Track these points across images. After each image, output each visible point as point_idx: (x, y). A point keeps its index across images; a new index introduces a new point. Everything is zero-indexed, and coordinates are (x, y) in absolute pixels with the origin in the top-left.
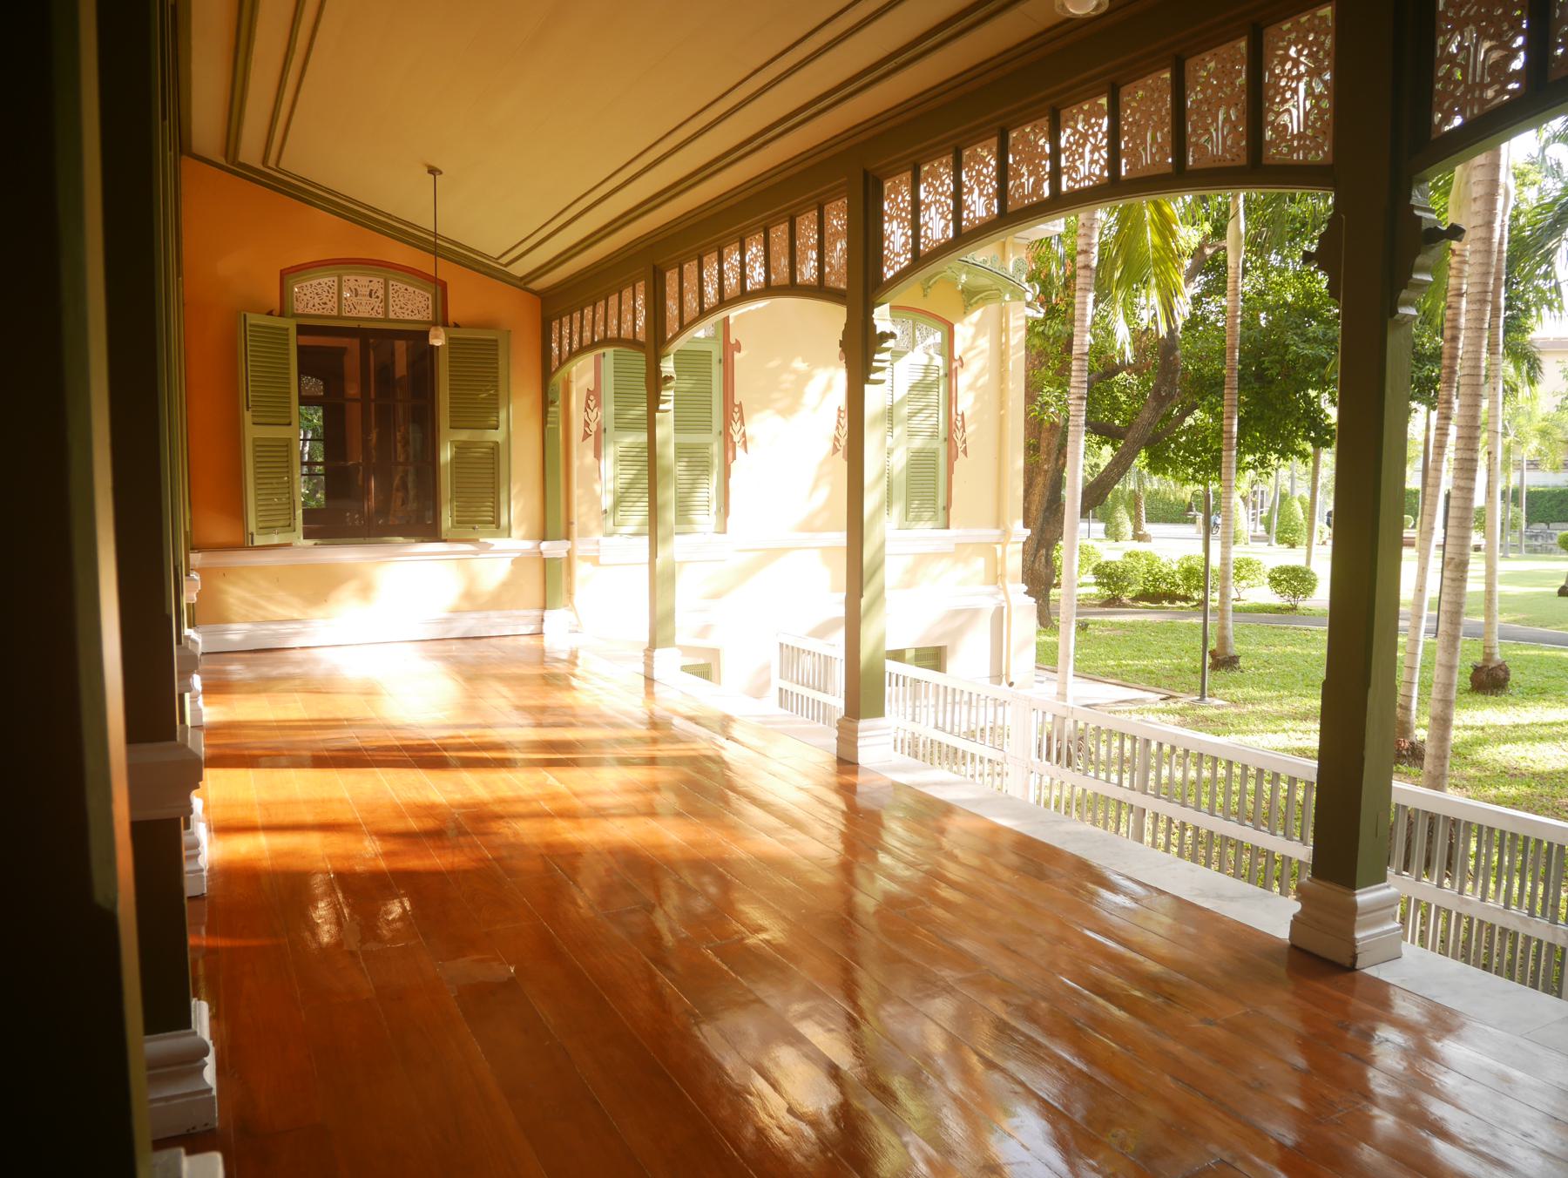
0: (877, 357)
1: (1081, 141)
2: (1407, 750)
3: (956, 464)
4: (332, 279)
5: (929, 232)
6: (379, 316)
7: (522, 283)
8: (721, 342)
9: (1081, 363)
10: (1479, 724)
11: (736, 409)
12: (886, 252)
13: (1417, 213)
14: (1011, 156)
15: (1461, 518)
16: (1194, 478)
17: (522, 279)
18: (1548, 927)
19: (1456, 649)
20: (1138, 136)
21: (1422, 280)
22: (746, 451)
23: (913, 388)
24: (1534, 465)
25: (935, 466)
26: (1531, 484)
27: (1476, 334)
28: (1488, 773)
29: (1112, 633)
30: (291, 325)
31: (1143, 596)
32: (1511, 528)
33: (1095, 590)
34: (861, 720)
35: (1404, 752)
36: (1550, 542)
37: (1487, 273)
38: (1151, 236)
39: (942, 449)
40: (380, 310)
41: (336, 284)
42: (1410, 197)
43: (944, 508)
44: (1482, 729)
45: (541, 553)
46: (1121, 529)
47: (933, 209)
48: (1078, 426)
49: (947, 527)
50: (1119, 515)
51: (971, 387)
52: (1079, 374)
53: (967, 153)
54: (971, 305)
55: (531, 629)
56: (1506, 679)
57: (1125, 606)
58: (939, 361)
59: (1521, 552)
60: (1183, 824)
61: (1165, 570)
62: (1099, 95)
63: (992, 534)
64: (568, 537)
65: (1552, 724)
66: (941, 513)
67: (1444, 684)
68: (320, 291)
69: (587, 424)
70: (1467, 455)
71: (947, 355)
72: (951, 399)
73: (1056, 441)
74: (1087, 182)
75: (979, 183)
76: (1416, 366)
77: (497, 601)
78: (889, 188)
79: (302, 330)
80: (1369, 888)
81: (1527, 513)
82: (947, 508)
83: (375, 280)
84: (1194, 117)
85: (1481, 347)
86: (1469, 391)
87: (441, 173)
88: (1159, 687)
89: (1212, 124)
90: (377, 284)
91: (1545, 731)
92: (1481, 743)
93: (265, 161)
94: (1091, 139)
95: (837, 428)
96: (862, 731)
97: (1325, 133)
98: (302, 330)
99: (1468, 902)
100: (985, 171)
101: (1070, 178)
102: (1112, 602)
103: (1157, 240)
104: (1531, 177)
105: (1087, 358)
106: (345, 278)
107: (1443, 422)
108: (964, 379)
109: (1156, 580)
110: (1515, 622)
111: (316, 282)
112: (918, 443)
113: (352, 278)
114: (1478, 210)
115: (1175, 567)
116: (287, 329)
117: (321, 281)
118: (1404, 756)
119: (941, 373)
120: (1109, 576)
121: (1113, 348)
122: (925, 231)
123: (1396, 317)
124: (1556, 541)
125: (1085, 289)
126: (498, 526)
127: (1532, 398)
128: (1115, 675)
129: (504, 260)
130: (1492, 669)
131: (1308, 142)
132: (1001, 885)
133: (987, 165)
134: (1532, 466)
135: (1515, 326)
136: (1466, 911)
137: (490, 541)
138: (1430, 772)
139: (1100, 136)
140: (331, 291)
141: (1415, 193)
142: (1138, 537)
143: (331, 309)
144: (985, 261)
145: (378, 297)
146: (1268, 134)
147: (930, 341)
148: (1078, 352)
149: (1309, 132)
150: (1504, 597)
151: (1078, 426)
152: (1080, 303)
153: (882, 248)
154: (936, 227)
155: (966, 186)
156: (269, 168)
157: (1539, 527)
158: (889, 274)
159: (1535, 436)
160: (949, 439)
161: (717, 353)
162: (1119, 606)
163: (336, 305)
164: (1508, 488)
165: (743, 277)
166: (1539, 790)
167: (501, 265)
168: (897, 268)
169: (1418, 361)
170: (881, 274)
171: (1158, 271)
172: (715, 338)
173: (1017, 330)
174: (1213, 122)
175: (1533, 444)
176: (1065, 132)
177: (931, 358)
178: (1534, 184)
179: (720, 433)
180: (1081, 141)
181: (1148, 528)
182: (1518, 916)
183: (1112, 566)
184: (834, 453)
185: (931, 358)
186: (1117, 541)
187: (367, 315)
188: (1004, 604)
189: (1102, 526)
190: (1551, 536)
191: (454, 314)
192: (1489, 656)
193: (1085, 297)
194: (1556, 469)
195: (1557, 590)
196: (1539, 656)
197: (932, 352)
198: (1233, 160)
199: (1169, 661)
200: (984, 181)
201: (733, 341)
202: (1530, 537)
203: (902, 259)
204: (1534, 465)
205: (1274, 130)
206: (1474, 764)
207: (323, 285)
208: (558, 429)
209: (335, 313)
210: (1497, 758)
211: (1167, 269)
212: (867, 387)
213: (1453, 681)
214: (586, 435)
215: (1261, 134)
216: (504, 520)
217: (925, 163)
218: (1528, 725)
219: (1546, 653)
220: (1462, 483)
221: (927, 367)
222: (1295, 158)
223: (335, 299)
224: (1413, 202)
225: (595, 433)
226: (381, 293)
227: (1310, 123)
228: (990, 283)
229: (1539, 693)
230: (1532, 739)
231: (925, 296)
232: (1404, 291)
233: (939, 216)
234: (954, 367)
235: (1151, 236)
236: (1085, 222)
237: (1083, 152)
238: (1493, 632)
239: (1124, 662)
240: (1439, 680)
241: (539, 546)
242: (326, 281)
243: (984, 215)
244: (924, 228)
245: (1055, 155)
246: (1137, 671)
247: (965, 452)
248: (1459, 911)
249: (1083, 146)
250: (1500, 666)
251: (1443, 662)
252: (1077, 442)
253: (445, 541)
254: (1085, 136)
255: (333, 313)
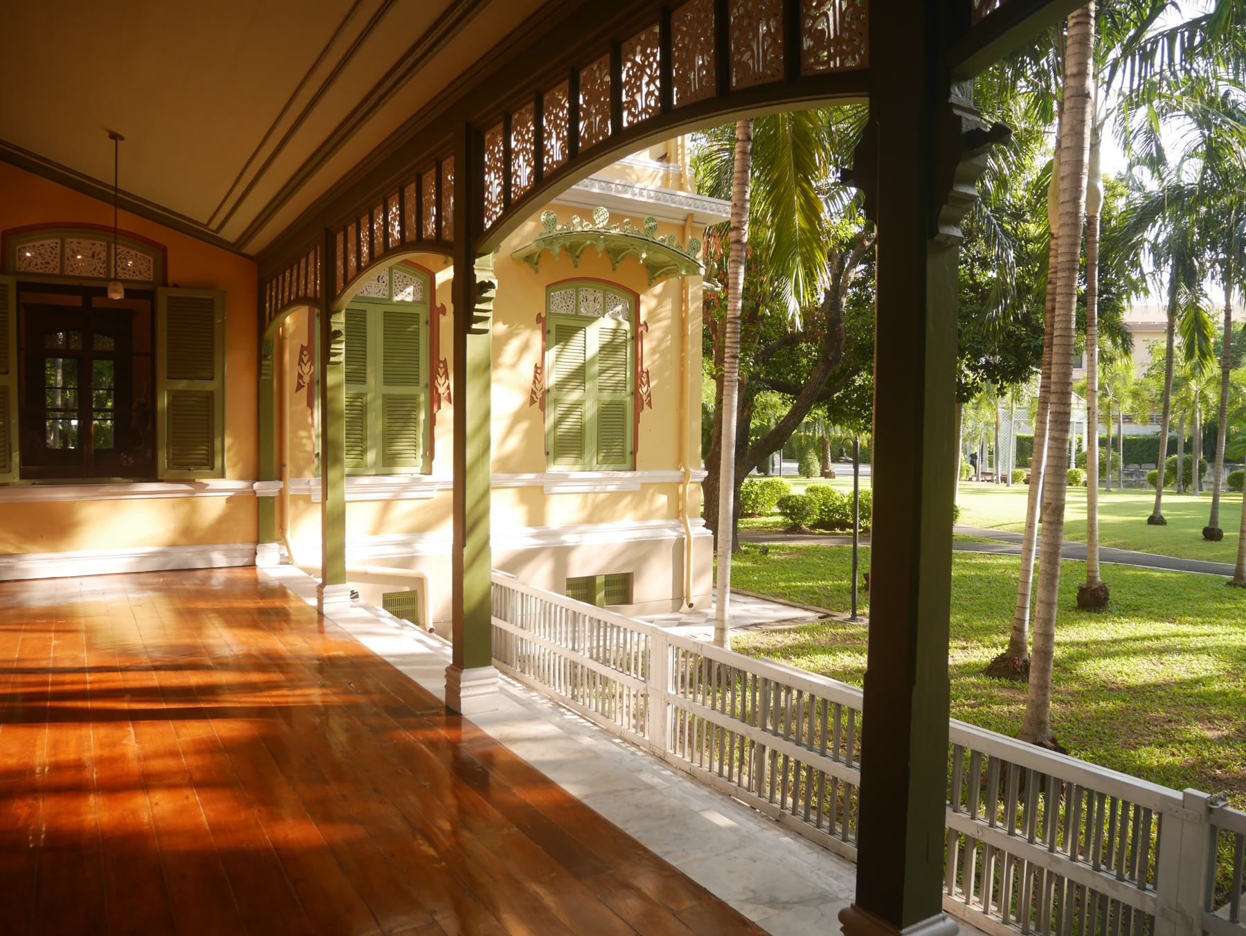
0: (477, 306)
1: (639, 73)
2: (1021, 667)
3: (642, 415)
4: (54, 241)
5: (518, 180)
6: (102, 276)
7: (235, 248)
8: (428, 306)
9: (734, 326)
10: (1084, 640)
11: (441, 365)
12: (486, 203)
13: (957, 112)
14: (581, 97)
15: (1057, 466)
16: (866, 428)
17: (234, 244)
18: (1137, 892)
19: (1054, 587)
20: (688, 63)
21: (966, 194)
22: (651, 408)
23: (603, 348)
24: (1128, 419)
25: (623, 417)
26: (1127, 433)
27: (1066, 299)
28: (1090, 687)
29: (788, 557)
30: (11, 282)
31: (820, 524)
32: (1112, 468)
33: (780, 519)
34: (465, 670)
35: (1019, 669)
36: (1142, 478)
37: (1074, 245)
38: (798, 220)
39: (629, 400)
40: (102, 271)
41: (59, 246)
42: (949, 94)
43: (631, 452)
44: (1086, 644)
45: (255, 492)
46: (812, 468)
47: (521, 158)
48: (732, 381)
49: (634, 469)
50: (809, 457)
51: (654, 351)
52: (733, 335)
53: (546, 97)
54: (655, 278)
55: (246, 561)
56: (1106, 599)
57: (804, 532)
58: (626, 326)
59: (1120, 487)
60: (798, 763)
61: (838, 503)
62: (652, 24)
63: (672, 475)
64: (280, 478)
65: (1143, 639)
66: (629, 458)
67: (1044, 619)
68: (43, 252)
69: (300, 377)
70: (1060, 409)
71: (633, 320)
72: (637, 359)
74: (644, 116)
75: (556, 126)
76: (1033, 337)
77: (217, 534)
78: (489, 139)
79: (22, 287)
80: (919, 924)
81: (1124, 457)
82: (634, 452)
83: (98, 243)
84: (736, 34)
85: (1071, 310)
86: (1061, 351)
87: (122, 139)
88: (819, 606)
89: (753, 39)
90: (100, 247)
91: (1138, 645)
92: (1084, 657)
94: (648, 71)
95: (534, 382)
96: (464, 681)
97: (861, 35)
98: (22, 287)
99: (1058, 861)
100: (561, 115)
101: (630, 113)
102: (793, 530)
103: (805, 226)
104: (1119, 190)
105: (739, 321)
106: (68, 240)
107: (1046, 381)
108: (647, 345)
109: (830, 511)
110: (1115, 546)
111: (40, 243)
112: (607, 396)
113: (75, 241)
114: (1065, 187)
115: (846, 500)
116: (6, 286)
117: (43, 242)
118: (1019, 673)
119: (629, 336)
120: (791, 507)
121: (786, 319)
122: (515, 180)
123: (937, 238)
124: (1146, 478)
125: (737, 261)
126: (212, 468)
127: (1127, 367)
128: (783, 595)
129: (214, 226)
130: (1095, 590)
131: (844, 47)
133: (562, 108)
134: (1127, 420)
135: (1110, 307)
136: (1056, 869)
137: (205, 481)
138: (1032, 701)
139: (655, 65)
140: (54, 252)
141: (955, 90)
142: (826, 474)
143: (54, 267)
144: (663, 240)
145: (100, 259)
146: (807, 43)
147: (619, 308)
148: (731, 316)
149: (846, 35)
150: (1103, 525)
151: (732, 381)
152: (733, 273)
153: (483, 199)
154: (523, 173)
155: (546, 131)
157: (1133, 467)
158: (488, 225)
159: (1128, 396)
160: (635, 393)
161: (424, 316)
162: (799, 533)
163: (58, 265)
164: (1109, 436)
165: (386, 235)
166: (1133, 704)
167: (212, 230)
168: (494, 218)
169: (1034, 333)
170: (483, 225)
171: (804, 250)
172: (422, 302)
173: (694, 300)
174: (754, 37)
175: (1127, 405)
176: (625, 66)
177: (619, 323)
178: (1121, 195)
179: (427, 386)
180: (639, 73)
181: (833, 467)
182: (1106, 879)
183: (793, 500)
184: (531, 404)
185: (619, 323)
186: (808, 477)
187: (89, 275)
188: (685, 536)
189: (796, 465)
190: (1142, 474)
191: (173, 276)
192: (1092, 579)
193: (737, 268)
194: (1144, 423)
195: (1147, 518)
196: (1133, 576)
197: (620, 318)
198: (773, 76)
199: (831, 583)
200: (560, 124)
201: (438, 305)
202: (1127, 475)
203: (498, 210)
204: (1128, 419)
205: (812, 37)
206: (1078, 679)
207: (46, 246)
208: (272, 380)
209: (57, 271)
210: (1098, 672)
211: (812, 249)
212: (469, 336)
213: (1052, 616)
214: (300, 387)
215: (799, 43)
216: (218, 463)
217: (515, 112)
218: (1124, 640)
219: (1139, 573)
220: (1057, 435)
221: (615, 331)
222: (832, 66)
223: (58, 260)
224: (953, 99)
225: (308, 384)
226: (103, 255)
227: (846, 26)
228: (669, 259)
229: (1132, 610)
230: (1127, 653)
231: (614, 269)
232: (944, 206)
233: (525, 164)
234: (639, 332)
235: (798, 220)
236: (736, 202)
237: (641, 84)
238: (1095, 559)
239: (793, 584)
240: (1040, 616)
241: (252, 486)
242: (50, 243)
243: (561, 158)
244: (514, 176)
245: (617, 86)
246: (803, 591)
247: (650, 404)
248: (1050, 869)
249: (641, 78)
250: (1101, 587)
251: (1043, 599)
252: (731, 396)
253: (161, 481)
254: (642, 68)
255: (55, 272)
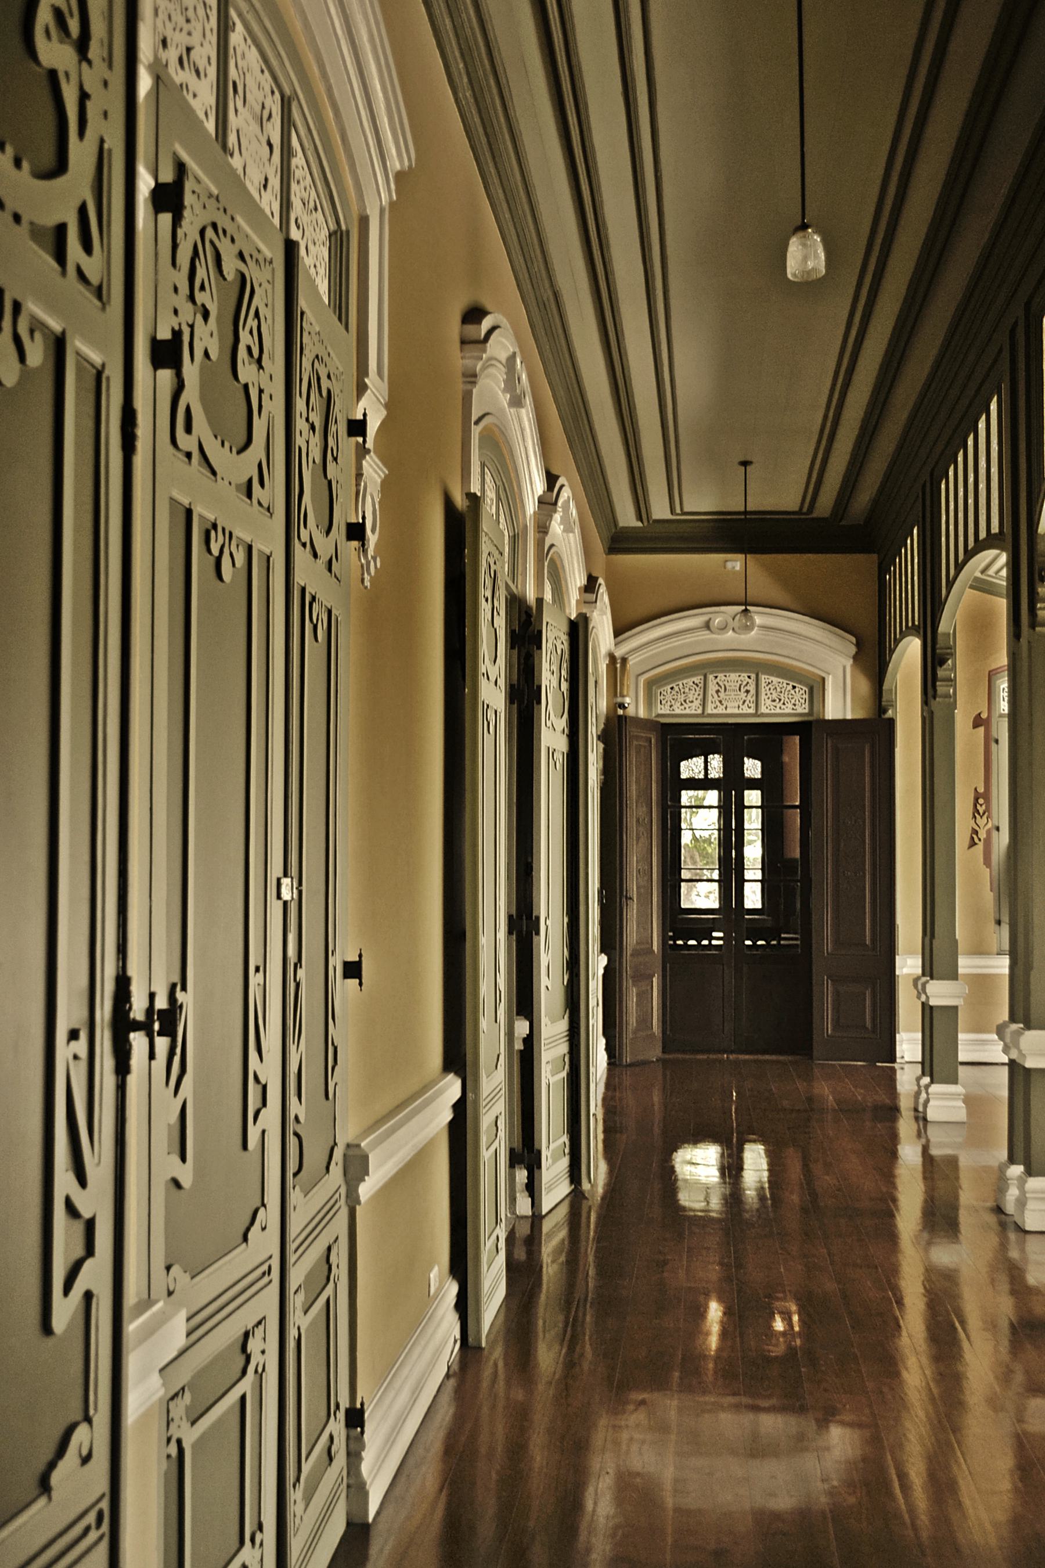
41: (702, 682)
73: (349, 1176)
93: (672, 511)
132: (80, 358)
156: (678, 514)
167: (805, 514)
214: (973, 844)
